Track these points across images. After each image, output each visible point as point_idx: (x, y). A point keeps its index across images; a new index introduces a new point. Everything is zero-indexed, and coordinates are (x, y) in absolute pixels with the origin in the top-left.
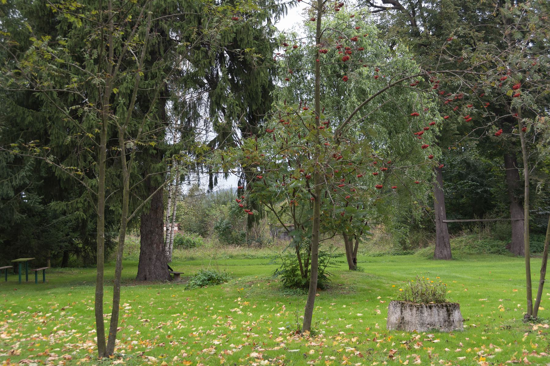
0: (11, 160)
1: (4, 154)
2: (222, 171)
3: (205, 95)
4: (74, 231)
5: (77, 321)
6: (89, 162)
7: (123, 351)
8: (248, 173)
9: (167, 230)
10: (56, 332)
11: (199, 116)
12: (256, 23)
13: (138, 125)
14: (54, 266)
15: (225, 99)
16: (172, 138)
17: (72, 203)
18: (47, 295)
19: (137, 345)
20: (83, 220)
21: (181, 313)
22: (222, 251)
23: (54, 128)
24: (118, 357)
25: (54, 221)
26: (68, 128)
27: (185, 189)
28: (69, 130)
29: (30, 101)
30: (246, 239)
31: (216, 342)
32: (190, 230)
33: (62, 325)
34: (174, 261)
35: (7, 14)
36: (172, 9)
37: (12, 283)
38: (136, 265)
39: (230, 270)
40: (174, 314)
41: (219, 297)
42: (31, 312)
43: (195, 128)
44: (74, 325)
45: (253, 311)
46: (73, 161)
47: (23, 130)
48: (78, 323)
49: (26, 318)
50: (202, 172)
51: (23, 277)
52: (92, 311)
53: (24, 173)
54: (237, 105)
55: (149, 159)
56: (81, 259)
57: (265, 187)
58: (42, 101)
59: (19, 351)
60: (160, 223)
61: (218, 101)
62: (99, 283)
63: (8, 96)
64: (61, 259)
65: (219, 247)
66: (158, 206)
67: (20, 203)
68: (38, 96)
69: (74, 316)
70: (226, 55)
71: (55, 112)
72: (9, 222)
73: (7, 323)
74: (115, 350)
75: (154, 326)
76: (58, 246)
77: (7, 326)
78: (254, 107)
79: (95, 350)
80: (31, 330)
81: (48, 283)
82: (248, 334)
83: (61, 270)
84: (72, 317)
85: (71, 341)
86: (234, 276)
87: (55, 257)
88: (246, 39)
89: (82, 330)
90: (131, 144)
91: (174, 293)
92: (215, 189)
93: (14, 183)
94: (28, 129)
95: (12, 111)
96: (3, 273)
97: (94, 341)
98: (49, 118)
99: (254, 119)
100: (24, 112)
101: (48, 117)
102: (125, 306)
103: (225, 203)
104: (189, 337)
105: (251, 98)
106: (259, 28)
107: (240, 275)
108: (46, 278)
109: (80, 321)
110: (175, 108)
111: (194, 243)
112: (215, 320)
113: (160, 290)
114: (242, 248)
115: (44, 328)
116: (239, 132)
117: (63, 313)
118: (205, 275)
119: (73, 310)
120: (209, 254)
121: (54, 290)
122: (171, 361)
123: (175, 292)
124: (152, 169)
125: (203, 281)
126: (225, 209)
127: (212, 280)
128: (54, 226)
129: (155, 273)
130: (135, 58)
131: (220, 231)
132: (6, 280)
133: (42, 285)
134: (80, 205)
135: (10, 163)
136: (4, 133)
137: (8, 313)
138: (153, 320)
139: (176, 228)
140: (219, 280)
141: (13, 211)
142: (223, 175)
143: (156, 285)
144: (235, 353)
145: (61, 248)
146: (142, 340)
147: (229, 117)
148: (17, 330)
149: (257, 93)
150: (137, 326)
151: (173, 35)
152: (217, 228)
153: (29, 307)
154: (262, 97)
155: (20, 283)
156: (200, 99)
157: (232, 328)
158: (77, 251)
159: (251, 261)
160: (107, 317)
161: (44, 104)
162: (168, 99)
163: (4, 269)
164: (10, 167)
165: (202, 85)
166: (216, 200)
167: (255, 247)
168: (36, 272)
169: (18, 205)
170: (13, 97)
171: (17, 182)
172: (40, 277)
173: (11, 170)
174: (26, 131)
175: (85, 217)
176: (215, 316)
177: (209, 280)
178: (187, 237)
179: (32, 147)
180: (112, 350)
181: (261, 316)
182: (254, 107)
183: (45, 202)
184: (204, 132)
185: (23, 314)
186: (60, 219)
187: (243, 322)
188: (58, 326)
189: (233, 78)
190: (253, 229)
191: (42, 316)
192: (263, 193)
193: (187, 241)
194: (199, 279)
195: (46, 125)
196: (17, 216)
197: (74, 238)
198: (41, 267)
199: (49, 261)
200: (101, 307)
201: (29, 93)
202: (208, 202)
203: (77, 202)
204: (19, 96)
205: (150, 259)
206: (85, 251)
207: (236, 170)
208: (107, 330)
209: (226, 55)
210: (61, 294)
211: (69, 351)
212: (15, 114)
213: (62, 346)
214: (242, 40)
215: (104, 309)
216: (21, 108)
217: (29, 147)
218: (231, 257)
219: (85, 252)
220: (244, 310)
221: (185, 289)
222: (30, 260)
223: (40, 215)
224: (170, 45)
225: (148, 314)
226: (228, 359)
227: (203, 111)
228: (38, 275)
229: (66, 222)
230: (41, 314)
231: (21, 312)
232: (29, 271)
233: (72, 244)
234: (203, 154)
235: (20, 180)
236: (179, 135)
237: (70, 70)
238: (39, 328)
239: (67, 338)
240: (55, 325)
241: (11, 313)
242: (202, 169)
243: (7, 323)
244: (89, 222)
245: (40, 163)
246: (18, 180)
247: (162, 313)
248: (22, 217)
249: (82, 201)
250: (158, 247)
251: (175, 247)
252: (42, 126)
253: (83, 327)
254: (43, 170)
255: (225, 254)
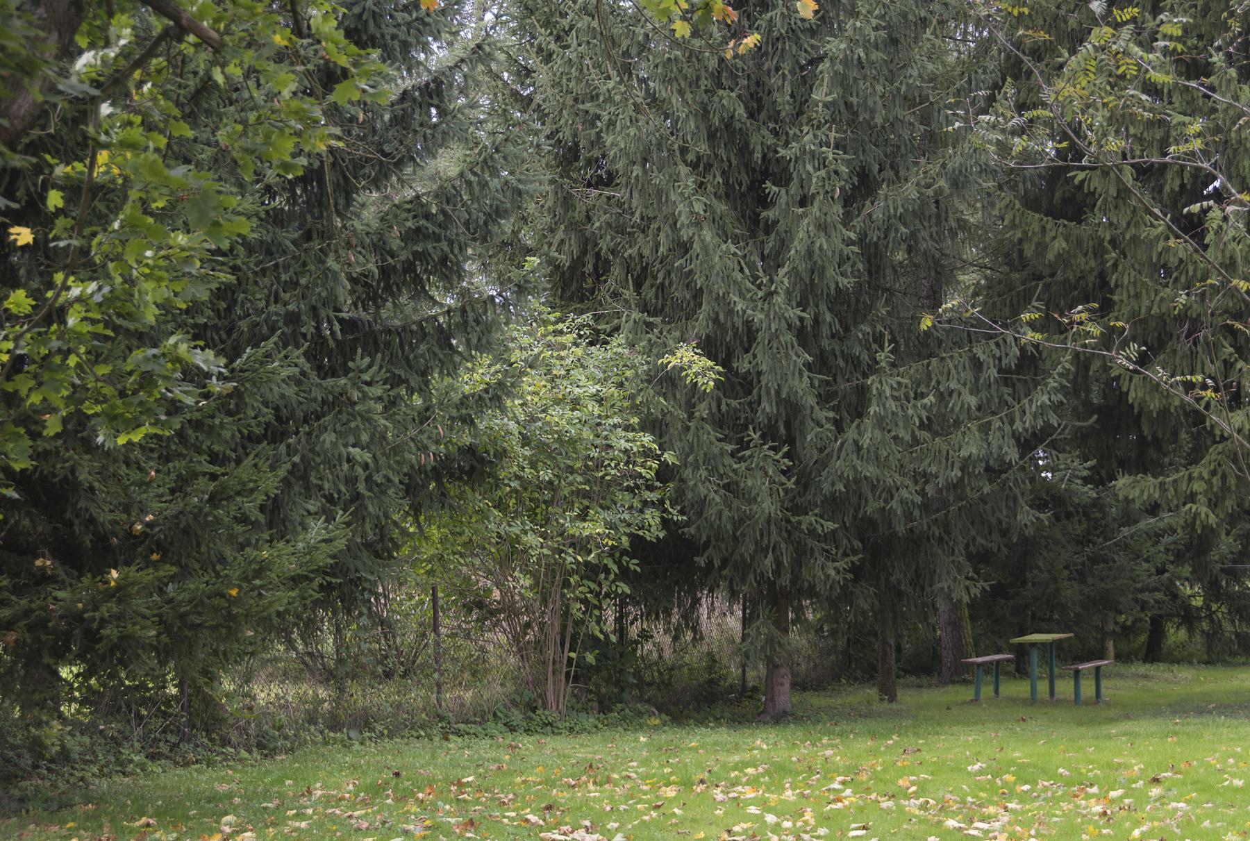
1: (993, 347)
4: (1179, 557)
5: (1198, 817)
6: (1225, 361)
17: (1175, 481)
23: (1125, 269)
25: (1126, 531)
26: (1164, 266)
28: (1165, 270)
29: (1058, 195)
33: (1156, 824)
37: (1013, 701)
42: (1069, 784)
46: (1178, 360)
47: (1040, 278)
48: (1199, 822)
49: (1055, 800)
51: (1043, 687)
53: (1045, 398)
56: (1198, 638)
58: (1093, 194)
63: (1000, 187)
64: (1143, 638)
67: (1032, 480)
68: (1083, 181)
69: (1187, 801)
71: (1129, 224)
72: (1005, 533)
73: (1006, 809)
76: (1136, 601)
77: (1006, 819)
81: (1108, 705)
83: (1142, 669)
84: (1182, 805)
87: (1127, 632)
93: (1018, 425)
94: (1053, 275)
96: (987, 672)
98: (1113, 242)
100: (1043, 229)
101: (1108, 237)
108: (1103, 691)
109: (1207, 816)
115: (1104, 831)
117: (1155, 791)
119: (1184, 783)
121: (1127, 726)
128: (1124, 546)
132: (997, 692)
133: (1094, 710)
134: (1198, 486)
136: (989, 288)
137: (1006, 783)
141: (1015, 499)
145: (1144, 606)
148: (1033, 832)
153: (1061, 770)
158: (1188, 617)
161: (1099, 203)
163: (991, 663)
164: (1006, 382)
168: (1077, 672)
169: (1029, 486)
170: (1014, 187)
172: (1088, 688)
173: (1010, 391)
174: (1048, 280)
175: (1213, 519)
179: (1081, 323)
183: (1099, 478)
185: (1046, 789)
188: (1144, 828)
191: (1098, 798)
195: (1103, 262)
196: (1026, 516)
197: (1179, 578)
198: (1089, 660)
199: (1110, 645)
201: (1056, 174)
203: (1190, 478)
204: (1029, 184)
206: (1210, 616)
210: (1148, 736)
212: (1019, 235)
216: (1037, 216)
217: (1072, 323)
219: (1212, 621)
222: (1060, 640)
223: (1085, 514)
228: (1082, 682)
229: (1157, 535)
230: (1095, 790)
232: (1056, 670)
235: (1035, 417)
237: (1170, 103)
238: (1091, 828)
240: (1137, 824)
241: (1015, 783)
243: (1006, 809)
244: (1223, 536)
245: (1087, 368)
248: (1038, 519)
249: (1206, 475)
252: (1092, 263)
254: (1095, 387)
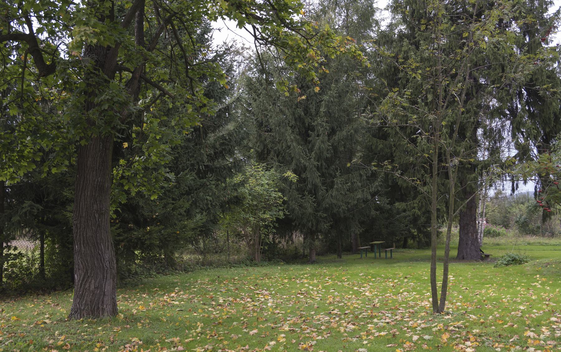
0: (369, 174)
2: (522, 179)
3: (508, 122)
7: (451, 310)
8: (544, 180)
9: (479, 223)
10: (402, 293)
11: (503, 138)
12: (548, 65)
13: (457, 147)
14: (397, 247)
15: (524, 125)
16: (482, 155)
18: (394, 267)
19: (460, 306)
20: (418, 215)
21: (492, 284)
22: (522, 239)
24: (448, 314)
25: (398, 216)
27: (492, 193)
29: (381, 134)
30: (540, 230)
31: (522, 308)
32: (495, 223)
34: (484, 246)
35: (366, 76)
36: (481, 62)
37: (370, 258)
38: (455, 248)
39: (528, 253)
40: (487, 284)
41: (521, 273)
43: (500, 147)
44: (414, 289)
45: (549, 285)
47: (376, 154)
50: (506, 180)
51: (378, 254)
52: (426, 280)
54: (533, 129)
55: (465, 171)
56: (416, 242)
57: (557, 190)
59: (378, 305)
60: (473, 218)
61: (518, 127)
62: (433, 260)
63: (366, 132)
64: (402, 242)
65: (519, 236)
66: (472, 206)
67: (375, 204)
70: (524, 92)
74: (445, 308)
75: (472, 293)
78: (548, 130)
79: (430, 307)
80: (385, 291)
82: (547, 303)
83: (402, 250)
85: (413, 300)
86: (533, 259)
87: (398, 241)
88: (540, 78)
89: (420, 293)
90: (456, 161)
91: (486, 270)
92: (516, 192)
95: (369, 141)
96: (364, 251)
97: (429, 301)
99: (547, 139)
102: (451, 277)
103: (523, 203)
104: (500, 303)
105: (545, 124)
106: (551, 69)
107: (537, 258)
110: (485, 133)
111: (499, 233)
112: (520, 291)
113: (475, 267)
114: (537, 237)
116: (535, 151)
117: (406, 280)
118: (509, 256)
120: (510, 241)
121: (399, 264)
122: (487, 320)
123: (487, 268)
124: (470, 179)
125: (508, 261)
126: (523, 207)
127: (515, 261)
129: (470, 254)
130: (458, 99)
131: (519, 224)
133: (390, 260)
134: (416, 205)
135: (369, 177)
137: (369, 278)
138: (471, 289)
139: (485, 222)
140: (521, 261)
142: (522, 182)
143: (471, 263)
144: (537, 317)
145: (402, 235)
146: (464, 302)
147: (527, 138)
149: (549, 119)
150: (460, 292)
151: (482, 81)
152: (517, 222)
154: (554, 122)
155: (375, 258)
156: (503, 126)
157: (533, 297)
158: (413, 237)
159: (545, 248)
160: (439, 284)
162: (478, 128)
164: (368, 180)
165: (505, 115)
166: (516, 201)
167: (549, 236)
171: (373, 190)
172: (389, 255)
175: (419, 213)
176: (519, 288)
177: (513, 261)
178: (494, 228)
180: (443, 308)
181: (557, 290)
182: (548, 130)
183: (391, 203)
184: (507, 150)
185: (379, 280)
186: (402, 215)
187: (542, 294)
189: (529, 108)
190: (546, 223)
191: (392, 282)
192: (556, 195)
193: (494, 231)
194: (505, 260)
199: (394, 244)
200: (435, 277)
201: (380, 128)
202: (510, 202)
205: (467, 244)
207: (533, 178)
208: (439, 292)
209: (524, 92)
210: (404, 266)
211: (412, 307)
213: (407, 303)
214: (537, 79)
215: (437, 278)
218: (529, 244)
220: (543, 284)
221: (494, 267)
224: (481, 88)
225: (468, 284)
226: (532, 321)
227: (507, 135)
228: (388, 253)
230: (391, 280)
231: (378, 278)
233: (410, 232)
234: (507, 166)
236: (486, 153)
239: (410, 298)
240: (401, 288)
242: (506, 178)
245: (388, 176)
246: (373, 188)
247: (478, 284)
250: (472, 235)
251: (484, 236)
253: (421, 291)
255: (524, 241)
